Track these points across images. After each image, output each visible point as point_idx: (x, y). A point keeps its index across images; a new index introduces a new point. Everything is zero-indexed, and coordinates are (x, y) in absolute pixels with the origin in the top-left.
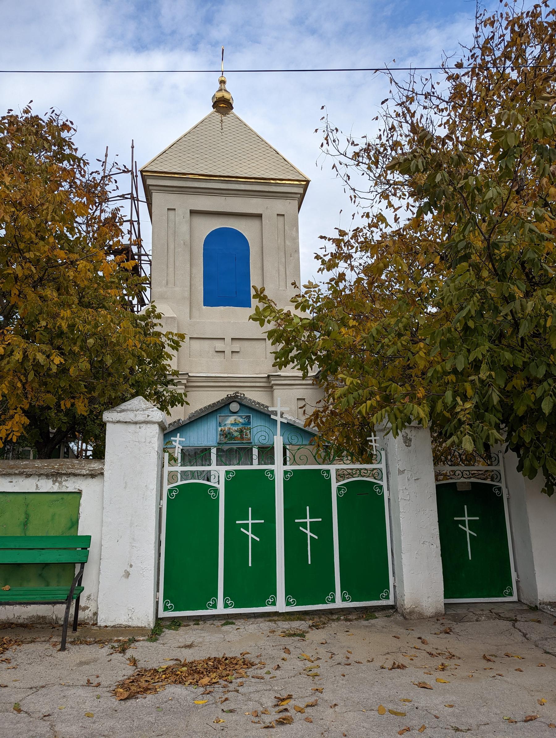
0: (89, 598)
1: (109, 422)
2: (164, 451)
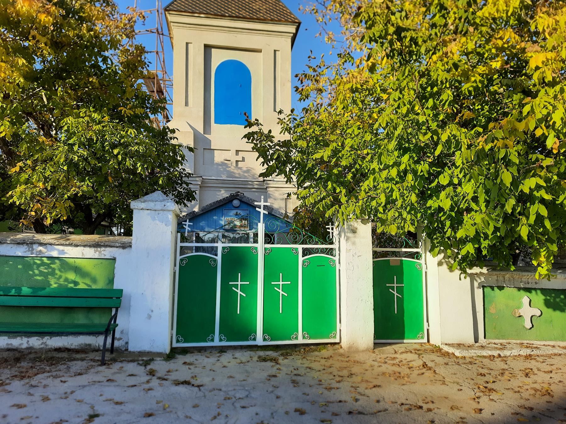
0: (122, 332)
2: (178, 232)
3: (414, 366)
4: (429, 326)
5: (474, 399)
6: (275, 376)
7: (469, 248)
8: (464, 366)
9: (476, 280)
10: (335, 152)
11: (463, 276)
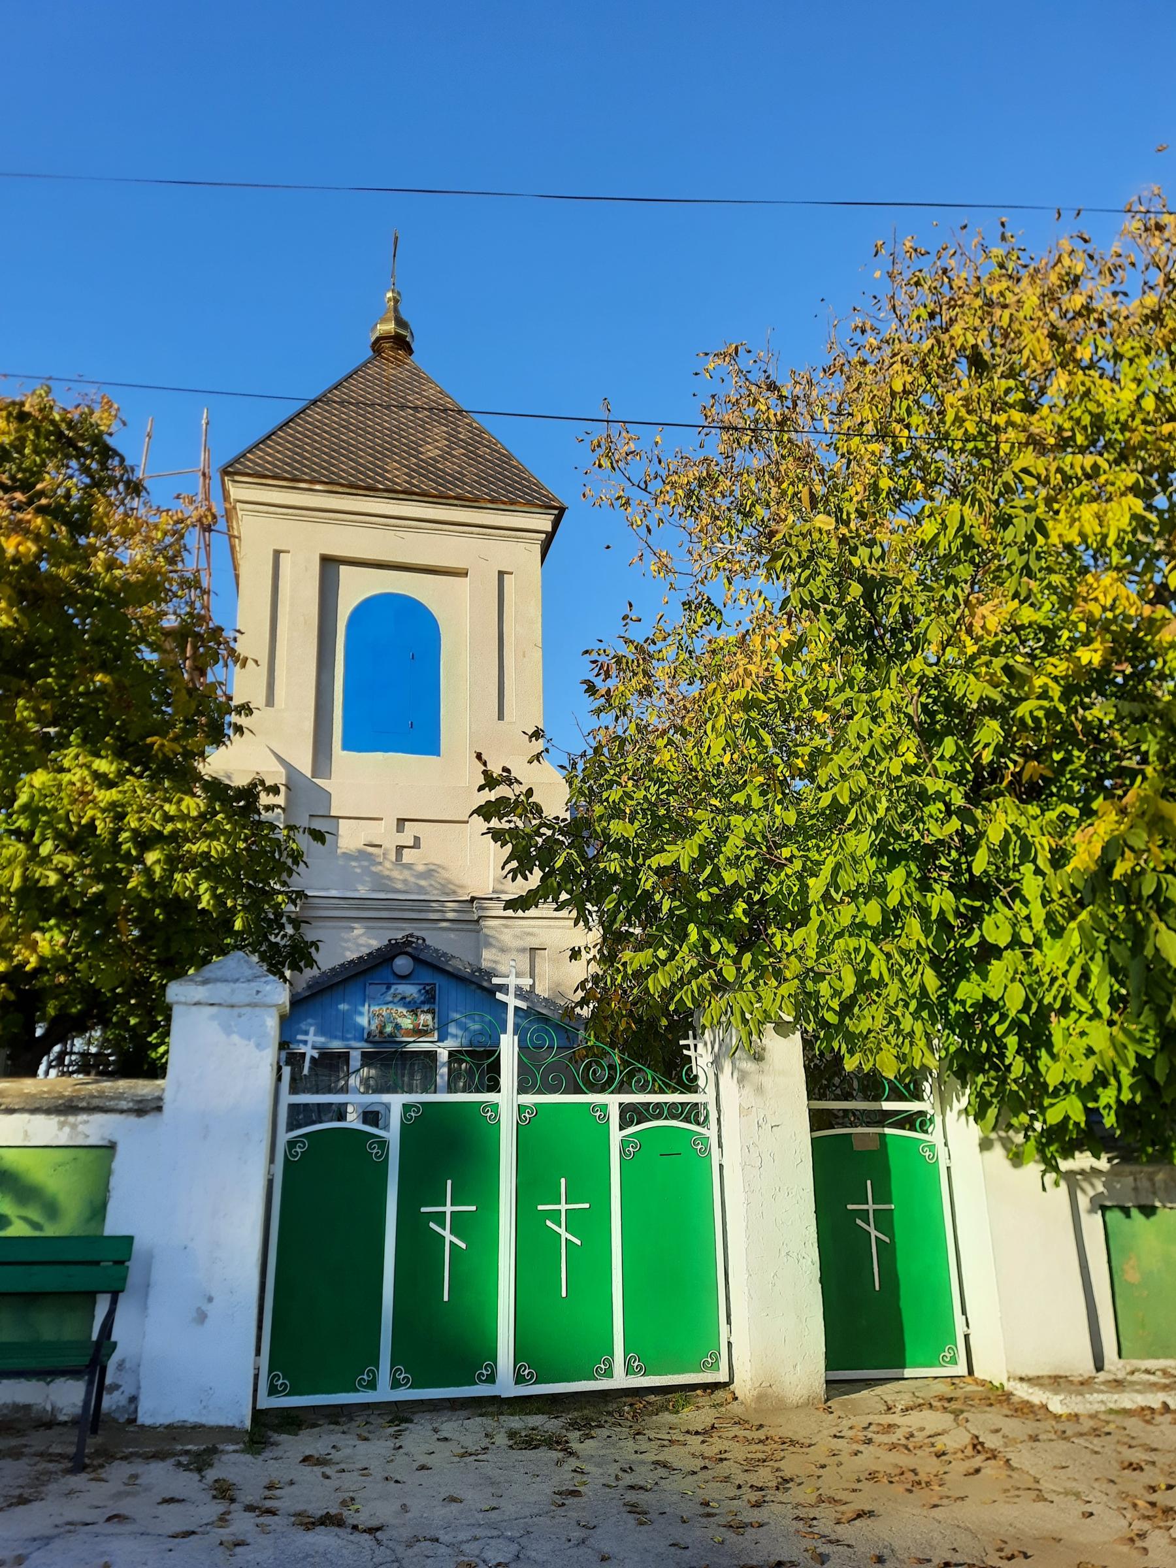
0: (121, 1366)
1: (178, 1003)
3: (950, 1450)
4: (968, 1326)
5: (1132, 1540)
6: (575, 1493)
7: (1071, 1109)
8: (1080, 1441)
9: (1083, 1190)
10: (707, 854)
11: (1051, 1177)
